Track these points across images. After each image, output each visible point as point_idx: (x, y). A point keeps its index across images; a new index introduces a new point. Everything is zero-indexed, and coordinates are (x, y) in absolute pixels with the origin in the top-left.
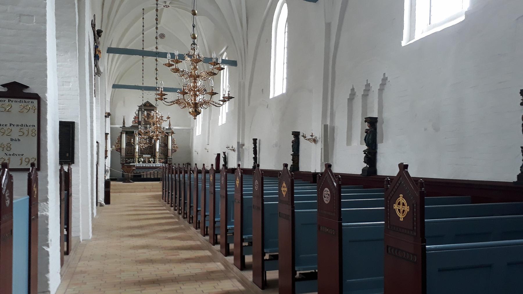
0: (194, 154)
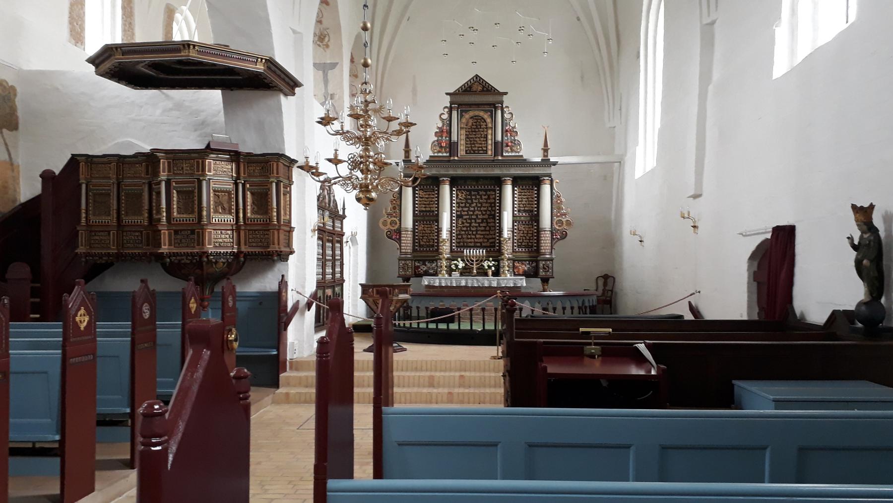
0: (628, 244)
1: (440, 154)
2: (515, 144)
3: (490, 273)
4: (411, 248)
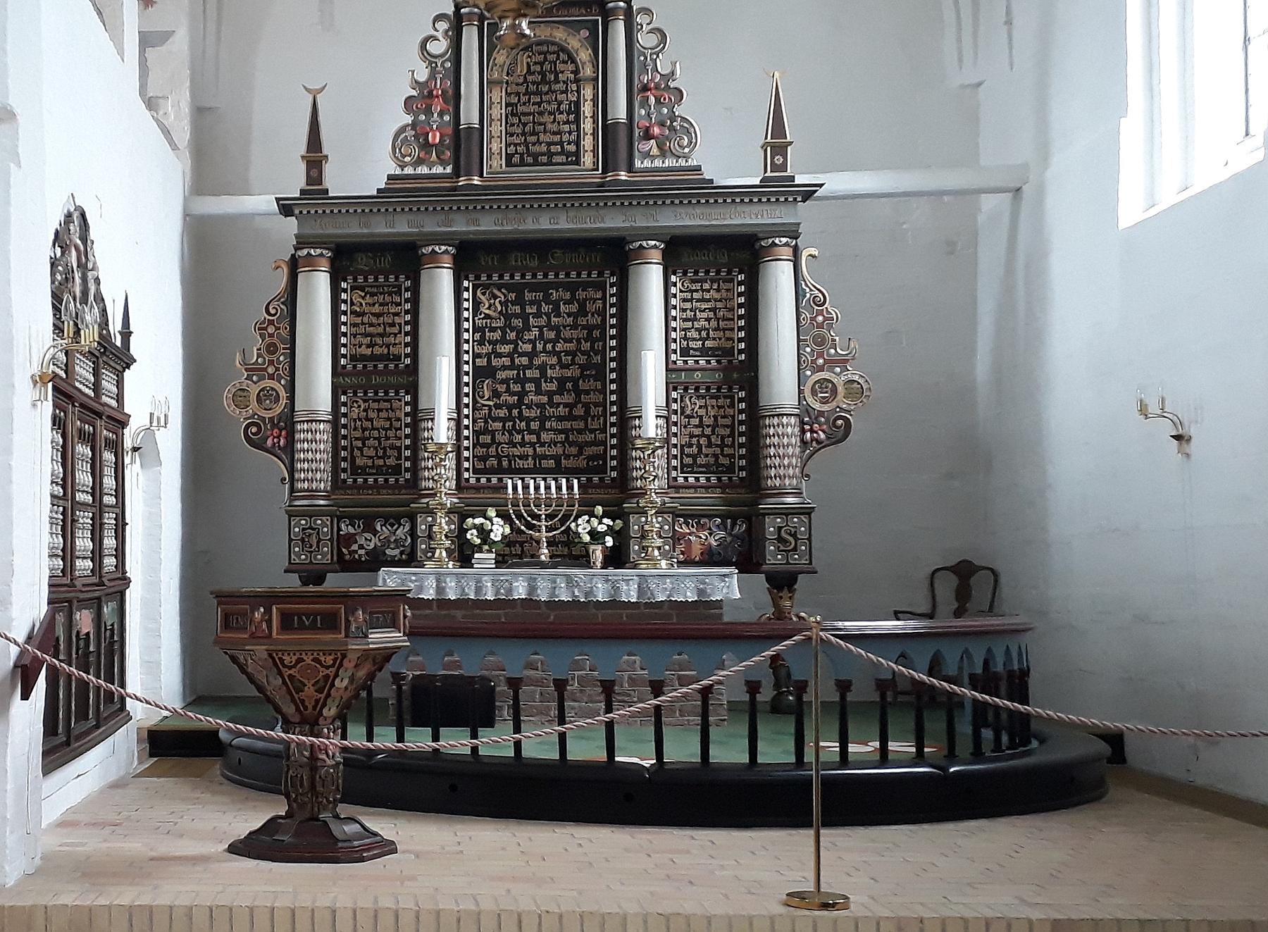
1: (423, 170)
2: (675, 131)
3: (598, 554)
4: (327, 476)
